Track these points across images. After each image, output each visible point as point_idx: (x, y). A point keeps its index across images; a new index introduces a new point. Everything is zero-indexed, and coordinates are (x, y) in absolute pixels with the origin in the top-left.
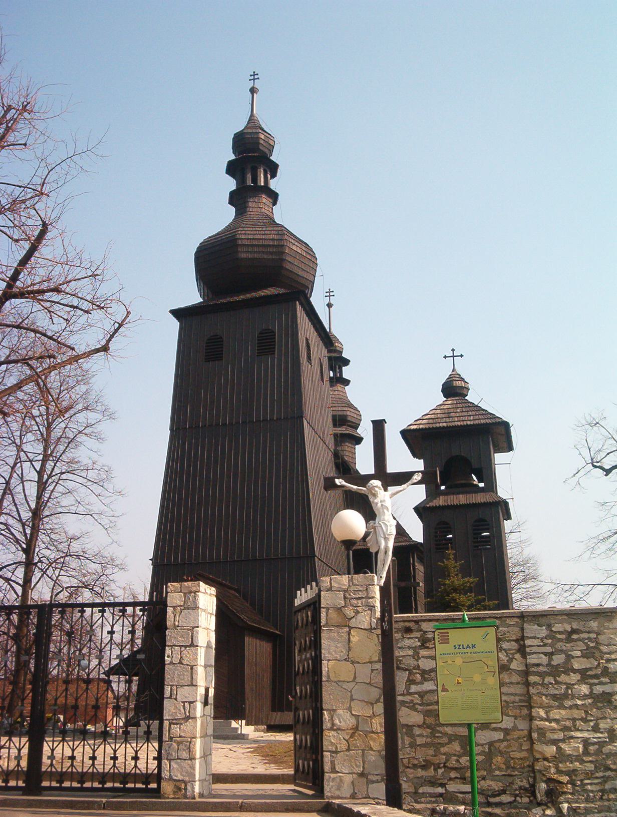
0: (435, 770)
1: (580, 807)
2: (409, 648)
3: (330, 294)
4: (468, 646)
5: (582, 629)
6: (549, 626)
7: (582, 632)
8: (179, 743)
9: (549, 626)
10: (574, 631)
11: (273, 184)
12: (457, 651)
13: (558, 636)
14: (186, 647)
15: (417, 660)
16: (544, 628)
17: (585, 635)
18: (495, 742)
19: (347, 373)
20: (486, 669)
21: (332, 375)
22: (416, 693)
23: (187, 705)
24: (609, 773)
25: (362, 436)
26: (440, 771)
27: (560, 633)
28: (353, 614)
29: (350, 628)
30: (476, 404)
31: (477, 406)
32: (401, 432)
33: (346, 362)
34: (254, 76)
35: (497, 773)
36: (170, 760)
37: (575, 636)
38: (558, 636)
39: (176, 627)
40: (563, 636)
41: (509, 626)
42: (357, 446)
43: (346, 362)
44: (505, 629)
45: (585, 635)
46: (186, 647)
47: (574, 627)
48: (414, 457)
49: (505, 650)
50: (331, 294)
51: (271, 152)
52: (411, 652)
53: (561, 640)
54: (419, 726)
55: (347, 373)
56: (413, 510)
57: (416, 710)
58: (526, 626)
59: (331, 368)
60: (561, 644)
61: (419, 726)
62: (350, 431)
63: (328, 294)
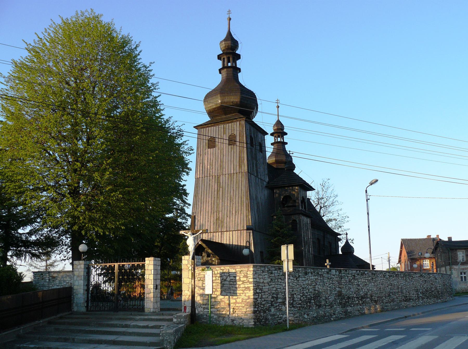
10: (241, 271)
14: (150, 274)
17: (244, 272)
27: (238, 271)
33: (286, 134)
37: (241, 272)
39: (148, 270)
42: (294, 171)
43: (286, 134)
45: (244, 272)
46: (150, 274)
50: (278, 101)
63: (277, 102)
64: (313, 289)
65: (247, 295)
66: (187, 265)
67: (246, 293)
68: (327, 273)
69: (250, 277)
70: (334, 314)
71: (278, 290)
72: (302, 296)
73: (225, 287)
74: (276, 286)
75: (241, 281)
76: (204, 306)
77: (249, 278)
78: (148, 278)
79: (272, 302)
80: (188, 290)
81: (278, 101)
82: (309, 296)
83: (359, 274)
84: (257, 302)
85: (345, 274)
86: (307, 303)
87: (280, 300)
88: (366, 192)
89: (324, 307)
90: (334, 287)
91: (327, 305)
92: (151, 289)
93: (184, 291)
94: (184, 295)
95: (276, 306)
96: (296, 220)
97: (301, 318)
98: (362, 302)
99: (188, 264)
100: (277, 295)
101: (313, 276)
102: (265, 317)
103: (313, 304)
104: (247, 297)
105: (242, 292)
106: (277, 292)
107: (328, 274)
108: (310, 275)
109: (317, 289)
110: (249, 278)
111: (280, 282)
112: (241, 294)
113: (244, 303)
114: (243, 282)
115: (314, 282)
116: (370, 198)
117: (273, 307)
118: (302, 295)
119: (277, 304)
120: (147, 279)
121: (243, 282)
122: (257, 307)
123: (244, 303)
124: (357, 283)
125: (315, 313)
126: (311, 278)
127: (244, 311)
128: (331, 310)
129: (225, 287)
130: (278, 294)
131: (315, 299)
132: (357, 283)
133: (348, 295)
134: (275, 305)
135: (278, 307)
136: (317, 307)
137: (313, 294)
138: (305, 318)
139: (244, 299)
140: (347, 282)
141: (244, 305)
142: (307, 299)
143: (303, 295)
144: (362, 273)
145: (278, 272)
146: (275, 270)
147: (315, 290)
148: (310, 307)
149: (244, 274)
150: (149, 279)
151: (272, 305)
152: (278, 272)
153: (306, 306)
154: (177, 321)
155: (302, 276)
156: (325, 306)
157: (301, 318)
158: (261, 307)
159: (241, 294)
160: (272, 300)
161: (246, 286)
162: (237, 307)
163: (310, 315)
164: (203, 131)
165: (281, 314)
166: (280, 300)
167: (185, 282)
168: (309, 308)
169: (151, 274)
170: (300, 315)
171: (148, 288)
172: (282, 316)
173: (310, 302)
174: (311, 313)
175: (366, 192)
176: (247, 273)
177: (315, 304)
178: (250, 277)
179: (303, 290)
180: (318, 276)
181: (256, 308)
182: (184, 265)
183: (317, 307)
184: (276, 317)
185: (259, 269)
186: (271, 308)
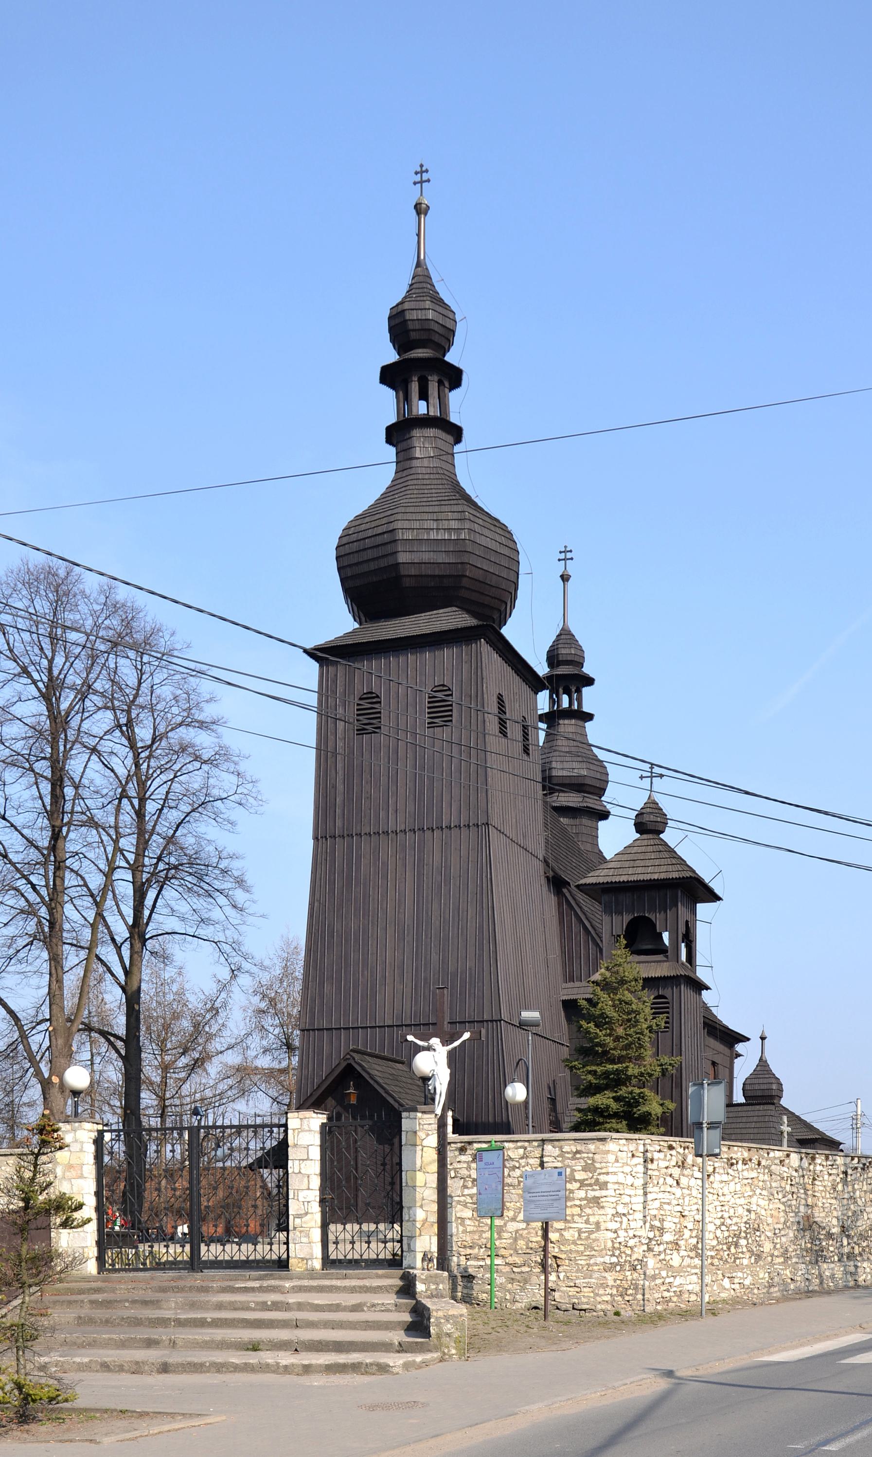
2: (465, 1162)
5: (584, 1150)
6: (561, 1148)
9: (561, 1148)
10: (578, 1152)
12: (486, 1167)
14: (303, 1160)
17: (585, 1155)
23: (306, 1203)
24: (593, 1253)
27: (568, 1153)
28: (424, 1137)
35: (520, 1252)
37: (578, 1156)
38: (567, 1155)
39: (295, 1145)
40: (570, 1156)
46: (303, 1160)
47: (578, 1149)
50: (569, 555)
52: (465, 1165)
53: (569, 1159)
57: (467, 1207)
63: (562, 556)
64: (746, 1207)
65: (592, 1219)
67: (588, 1215)
68: (781, 1162)
69: (601, 1169)
70: (792, 1279)
71: (666, 1207)
72: (719, 1227)
74: (661, 1195)
75: (576, 1181)
76: (468, 1251)
77: (599, 1171)
78: (297, 1171)
79: (650, 1239)
81: (569, 555)
82: (736, 1228)
83: (856, 1168)
84: (619, 1240)
85: (823, 1165)
86: (730, 1246)
87: (668, 1237)
89: (769, 1259)
90: (794, 1202)
91: (776, 1253)
94: (408, 1221)
95: (660, 1253)
97: (715, 1288)
98: (861, 1249)
100: (662, 1221)
101: (748, 1170)
102: (634, 1282)
103: (745, 1250)
105: (577, 1210)
106: (662, 1212)
107: (783, 1166)
108: (740, 1166)
109: (754, 1207)
110: (599, 1171)
111: (671, 1186)
112: (576, 1218)
114: (582, 1184)
115: (748, 1189)
117: (651, 1253)
118: (718, 1222)
119: (662, 1248)
120: (293, 1172)
121: (582, 1184)
122: (617, 1253)
124: (852, 1194)
125: (748, 1274)
126: (741, 1177)
128: (786, 1269)
130: (663, 1220)
131: (749, 1236)
132: (852, 1194)
133: (827, 1228)
134: (656, 1249)
135: (662, 1256)
136: (753, 1261)
137: (746, 1223)
138: (725, 1289)
139: (584, 1232)
140: (828, 1189)
141: (582, 1248)
142: (729, 1236)
143: (723, 1224)
144: (864, 1164)
145: (666, 1156)
146: (660, 1151)
147: (749, 1211)
148: (736, 1259)
149: (585, 1161)
150: (300, 1172)
151: (650, 1250)
152: (666, 1156)
153: (728, 1255)
155: (722, 1171)
156: (772, 1256)
157: (715, 1288)
158: (627, 1255)
159: (576, 1218)
160: (651, 1235)
161: (591, 1194)
162: (565, 1252)
163: (736, 1281)
164: (341, 670)
165: (670, 1274)
166: (668, 1237)
168: (734, 1262)
170: (714, 1279)
171: (298, 1200)
172: (671, 1280)
173: (737, 1245)
174: (740, 1274)
176: (593, 1159)
177: (749, 1251)
179: (723, 1208)
180: (759, 1171)
181: (614, 1256)
182: (407, 1132)
183: (753, 1258)
184: (658, 1281)
185: (625, 1148)
186: (646, 1257)
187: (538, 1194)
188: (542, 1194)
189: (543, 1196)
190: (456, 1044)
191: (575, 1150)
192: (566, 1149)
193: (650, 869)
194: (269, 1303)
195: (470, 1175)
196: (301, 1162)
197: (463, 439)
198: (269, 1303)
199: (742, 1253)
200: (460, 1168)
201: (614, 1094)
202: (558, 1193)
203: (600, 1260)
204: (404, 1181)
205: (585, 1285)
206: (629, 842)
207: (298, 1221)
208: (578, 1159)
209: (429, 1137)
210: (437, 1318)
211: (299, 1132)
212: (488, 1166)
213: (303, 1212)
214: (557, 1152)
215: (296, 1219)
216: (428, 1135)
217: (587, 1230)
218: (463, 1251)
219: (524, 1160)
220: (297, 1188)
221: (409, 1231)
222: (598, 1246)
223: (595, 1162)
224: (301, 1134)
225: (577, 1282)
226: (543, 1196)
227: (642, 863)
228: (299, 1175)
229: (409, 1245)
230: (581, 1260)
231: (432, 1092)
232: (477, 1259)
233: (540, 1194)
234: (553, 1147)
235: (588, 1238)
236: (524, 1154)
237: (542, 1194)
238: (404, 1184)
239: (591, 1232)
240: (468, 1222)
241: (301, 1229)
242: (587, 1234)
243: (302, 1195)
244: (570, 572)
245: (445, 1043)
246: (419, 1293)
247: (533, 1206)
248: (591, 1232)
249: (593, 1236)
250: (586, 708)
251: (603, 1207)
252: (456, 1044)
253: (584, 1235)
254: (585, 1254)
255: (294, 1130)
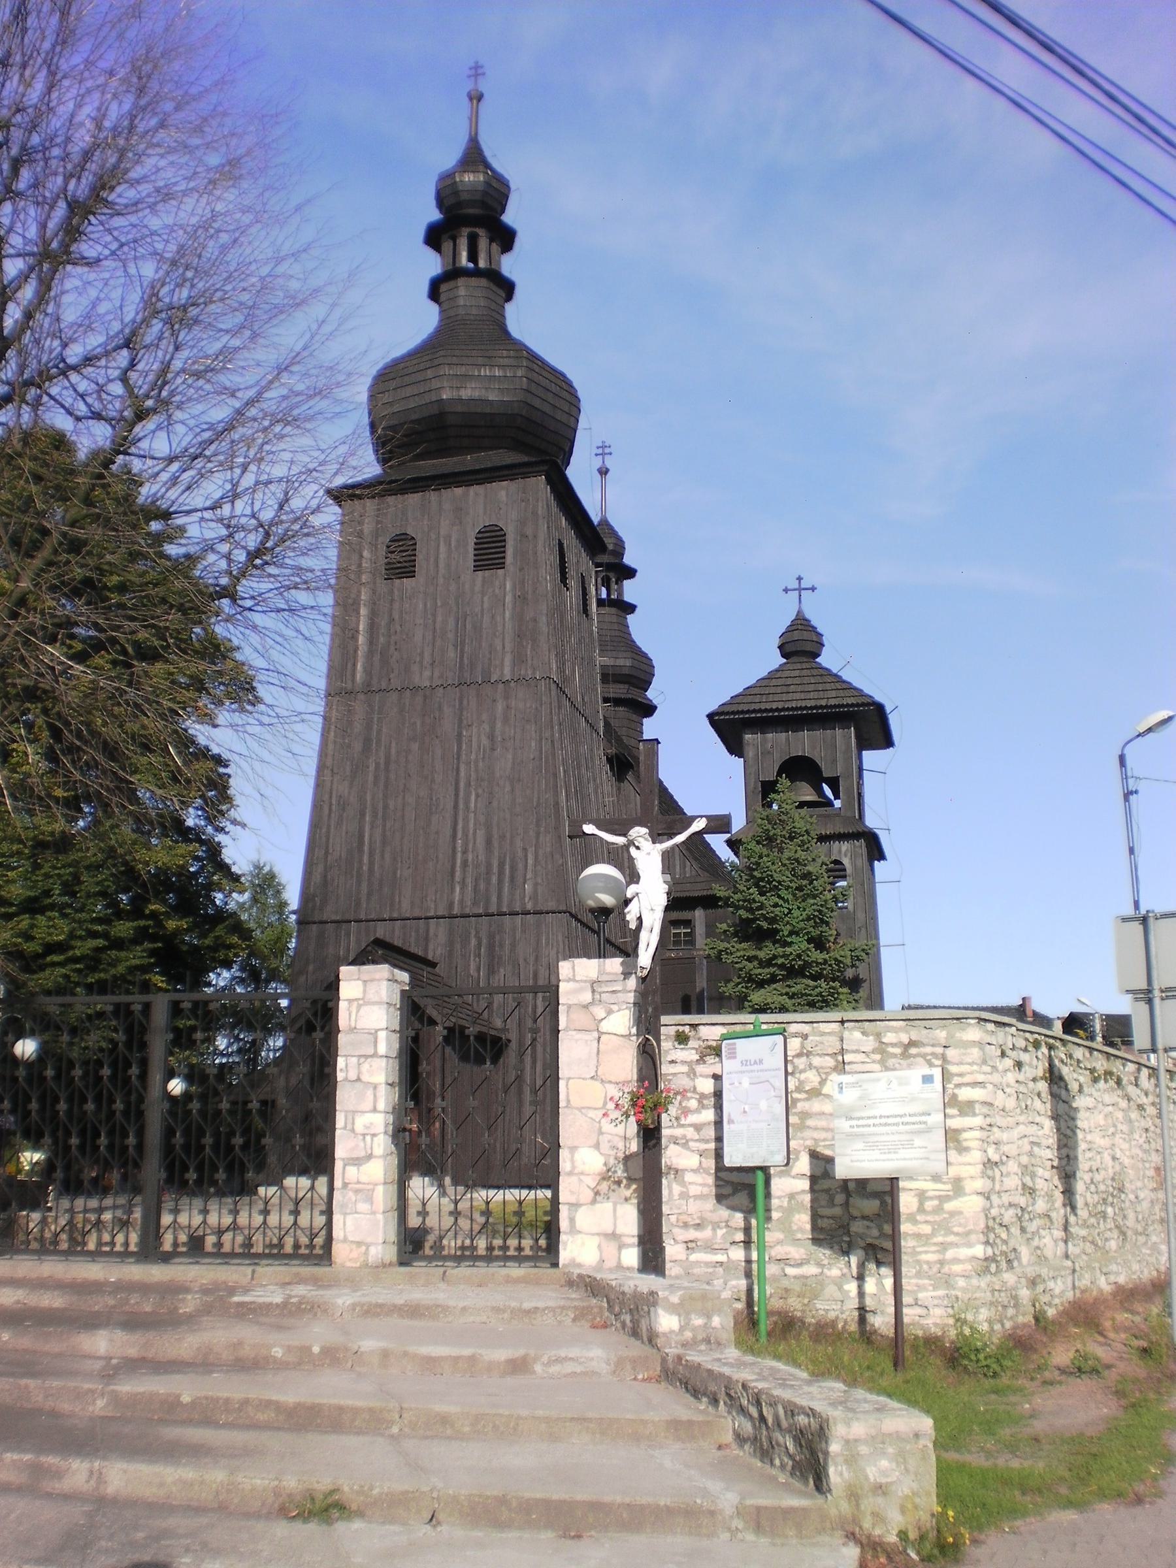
0: (714, 1229)
1: (934, 1290)
2: (684, 1062)
3: (604, 450)
4: (755, 1062)
5: (925, 1041)
6: (878, 1036)
7: (924, 1045)
8: (357, 1191)
9: (878, 1036)
10: (912, 1044)
11: (509, 265)
12: (744, 1068)
13: (891, 1050)
14: (366, 1057)
15: (693, 1080)
16: (871, 1038)
17: (928, 1049)
18: (797, 1193)
19: (630, 591)
20: (773, 1093)
21: (604, 595)
22: (690, 1125)
23: (368, 1138)
24: (951, 1238)
25: (655, 702)
26: (720, 1233)
27: (893, 1045)
28: (603, 1015)
29: (601, 1033)
30: (835, 671)
31: (836, 675)
32: (710, 717)
33: (630, 573)
34: (477, 71)
35: (799, 1236)
36: (345, 1214)
37: (913, 1051)
38: (891, 1050)
39: (353, 1030)
40: (898, 1051)
41: (823, 1034)
42: (645, 720)
43: (630, 573)
44: (817, 1038)
45: (928, 1049)
46: (366, 1057)
47: (913, 1038)
48: (731, 753)
49: (817, 1069)
50: (607, 450)
51: (503, 211)
52: (685, 1069)
53: (895, 1056)
54: (693, 1171)
55: (630, 591)
56: (725, 845)
57: (688, 1149)
58: (846, 1034)
59: (606, 583)
60: (893, 1060)
61: (693, 1171)
62: (633, 694)
63: (600, 451)
66: (586, 1007)
73: (816, 1129)
76: (692, 1234)
77: (957, 1080)
78: (352, 1075)
80: (597, 1146)
81: (607, 450)
88: (1122, 760)
92: (374, 1135)
93: (573, 1149)
94: (570, 1174)
96: (841, 863)
99: (592, 1003)
104: (949, 1187)
110: (957, 1080)
113: (929, 1218)
116: (1142, 786)
123: (929, 1218)
127: (928, 1263)
129: (816, 1129)
139: (931, 1198)
141: (927, 1229)
150: (359, 1079)
154: (682, 1329)
167: (575, 1101)
169: (375, 1055)
171: (353, 1130)
175: (1122, 760)
178: (961, 1075)
187: (871, 1122)
188: (883, 1121)
189: (886, 1124)
190: (680, 838)
191: (906, 1041)
192: (889, 1038)
193: (812, 695)
194: (316, 1349)
195: (695, 1088)
196: (362, 1060)
197: (514, 297)
198: (316, 1349)
199: (1110, 1230)
200: (675, 1074)
201: (788, 989)
202: (923, 1118)
203: (964, 1252)
204: (562, 1097)
205: (936, 1302)
206: (775, 666)
207: (352, 1171)
208: (915, 1056)
209: (612, 1017)
210: (847, 1442)
211: (359, 1007)
212: (749, 1068)
213: (362, 1154)
214: (869, 1043)
215: (348, 1168)
216: (610, 1012)
217: (937, 1193)
218: (682, 1235)
219: (804, 1059)
220: (351, 1108)
221: (572, 1192)
222: (960, 1225)
223: (949, 1062)
224: (364, 1009)
225: (920, 1295)
226: (886, 1124)
227: (800, 688)
228: (358, 1085)
229: (572, 1220)
230: (926, 1252)
231: (633, 926)
232: (710, 1248)
233: (877, 1121)
234: (863, 1033)
235: (938, 1210)
236: (803, 1047)
237: (883, 1121)
238: (562, 1104)
239: (943, 1199)
240: (689, 1177)
241: (358, 1186)
242: (936, 1202)
243: (360, 1123)
244: (608, 464)
245: (656, 837)
246: (665, 1334)
247: (860, 1145)
248: (943, 1199)
249: (949, 1206)
250: (628, 597)
251: (967, 1149)
252: (680, 838)
253: (929, 1205)
254: (935, 1240)
255: (350, 1001)
